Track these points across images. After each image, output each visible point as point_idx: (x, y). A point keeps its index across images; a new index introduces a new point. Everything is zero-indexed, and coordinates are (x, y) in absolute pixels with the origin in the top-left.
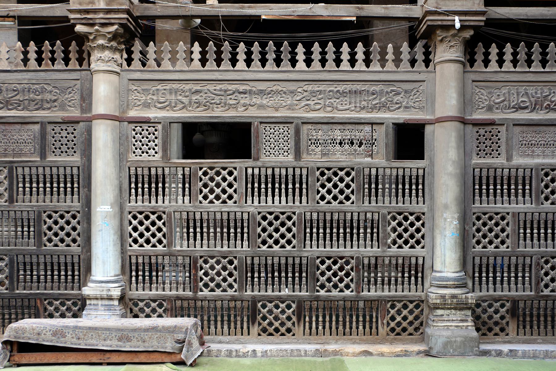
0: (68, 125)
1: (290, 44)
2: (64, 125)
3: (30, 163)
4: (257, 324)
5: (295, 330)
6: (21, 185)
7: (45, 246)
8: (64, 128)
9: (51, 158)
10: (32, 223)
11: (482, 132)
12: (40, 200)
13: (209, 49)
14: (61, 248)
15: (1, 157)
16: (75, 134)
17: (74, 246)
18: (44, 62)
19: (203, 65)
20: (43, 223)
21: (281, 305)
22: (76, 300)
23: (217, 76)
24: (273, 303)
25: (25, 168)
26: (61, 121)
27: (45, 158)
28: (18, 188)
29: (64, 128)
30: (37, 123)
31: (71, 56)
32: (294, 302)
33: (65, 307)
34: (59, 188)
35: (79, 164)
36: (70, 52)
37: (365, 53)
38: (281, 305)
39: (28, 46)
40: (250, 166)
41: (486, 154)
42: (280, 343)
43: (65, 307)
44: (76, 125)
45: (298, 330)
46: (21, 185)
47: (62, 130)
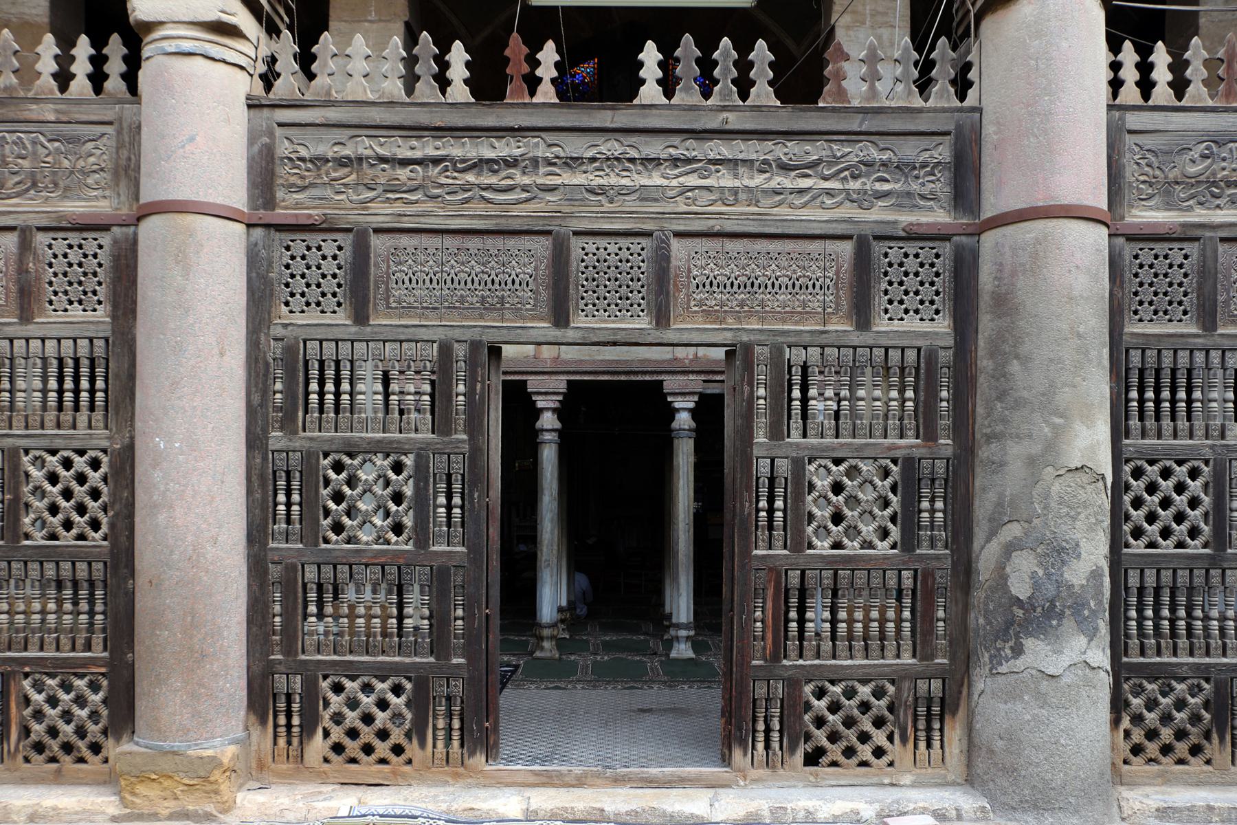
0: (85, 235)
1: (1139, 49)
2: (912, 244)
3: (319, 330)
4: (320, 732)
5: (412, 749)
6: (314, 386)
7: (326, 541)
8: (912, 251)
9: (882, 325)
10: (457, 487)
11: (299, 248)
12: (342, 425)
13: (757, 55)
14: (395, 547)
15: (3, 317)
16: (101, 259)
17: (397, 543)
18: (716, 89)
19: (669, 94)
20: (23, 478)
21: (348, 684)
22: (850, 683)
23: (734, 121)
24: (359, 681)
25: (15, 342)
26: (902, 234)
27: (1214, 327)
28: (307, 394)
29: (912, 251)
30: (849, 237)
31: (1155, 75)
32: (1207, 680)
33: (72, 695)
34: (1173, 402)
35: (108, 334)
36: (715, 64)
37: (92, 59)
38: (348, 684)
39: (106, 44)
40: (37, 335)
41: (1156, 312)
42: (1215, 784)
43: (72, 695)
44: (103, 234)
45: (1217, 750)
46: (314, 386)
47: (906, 255)
